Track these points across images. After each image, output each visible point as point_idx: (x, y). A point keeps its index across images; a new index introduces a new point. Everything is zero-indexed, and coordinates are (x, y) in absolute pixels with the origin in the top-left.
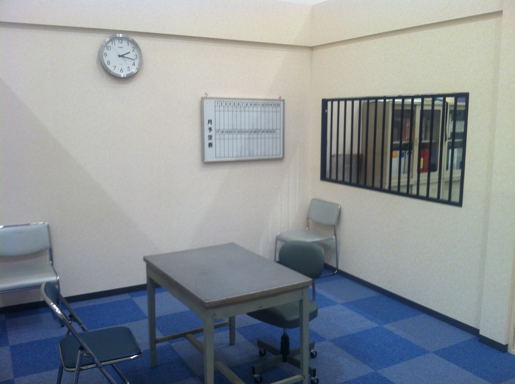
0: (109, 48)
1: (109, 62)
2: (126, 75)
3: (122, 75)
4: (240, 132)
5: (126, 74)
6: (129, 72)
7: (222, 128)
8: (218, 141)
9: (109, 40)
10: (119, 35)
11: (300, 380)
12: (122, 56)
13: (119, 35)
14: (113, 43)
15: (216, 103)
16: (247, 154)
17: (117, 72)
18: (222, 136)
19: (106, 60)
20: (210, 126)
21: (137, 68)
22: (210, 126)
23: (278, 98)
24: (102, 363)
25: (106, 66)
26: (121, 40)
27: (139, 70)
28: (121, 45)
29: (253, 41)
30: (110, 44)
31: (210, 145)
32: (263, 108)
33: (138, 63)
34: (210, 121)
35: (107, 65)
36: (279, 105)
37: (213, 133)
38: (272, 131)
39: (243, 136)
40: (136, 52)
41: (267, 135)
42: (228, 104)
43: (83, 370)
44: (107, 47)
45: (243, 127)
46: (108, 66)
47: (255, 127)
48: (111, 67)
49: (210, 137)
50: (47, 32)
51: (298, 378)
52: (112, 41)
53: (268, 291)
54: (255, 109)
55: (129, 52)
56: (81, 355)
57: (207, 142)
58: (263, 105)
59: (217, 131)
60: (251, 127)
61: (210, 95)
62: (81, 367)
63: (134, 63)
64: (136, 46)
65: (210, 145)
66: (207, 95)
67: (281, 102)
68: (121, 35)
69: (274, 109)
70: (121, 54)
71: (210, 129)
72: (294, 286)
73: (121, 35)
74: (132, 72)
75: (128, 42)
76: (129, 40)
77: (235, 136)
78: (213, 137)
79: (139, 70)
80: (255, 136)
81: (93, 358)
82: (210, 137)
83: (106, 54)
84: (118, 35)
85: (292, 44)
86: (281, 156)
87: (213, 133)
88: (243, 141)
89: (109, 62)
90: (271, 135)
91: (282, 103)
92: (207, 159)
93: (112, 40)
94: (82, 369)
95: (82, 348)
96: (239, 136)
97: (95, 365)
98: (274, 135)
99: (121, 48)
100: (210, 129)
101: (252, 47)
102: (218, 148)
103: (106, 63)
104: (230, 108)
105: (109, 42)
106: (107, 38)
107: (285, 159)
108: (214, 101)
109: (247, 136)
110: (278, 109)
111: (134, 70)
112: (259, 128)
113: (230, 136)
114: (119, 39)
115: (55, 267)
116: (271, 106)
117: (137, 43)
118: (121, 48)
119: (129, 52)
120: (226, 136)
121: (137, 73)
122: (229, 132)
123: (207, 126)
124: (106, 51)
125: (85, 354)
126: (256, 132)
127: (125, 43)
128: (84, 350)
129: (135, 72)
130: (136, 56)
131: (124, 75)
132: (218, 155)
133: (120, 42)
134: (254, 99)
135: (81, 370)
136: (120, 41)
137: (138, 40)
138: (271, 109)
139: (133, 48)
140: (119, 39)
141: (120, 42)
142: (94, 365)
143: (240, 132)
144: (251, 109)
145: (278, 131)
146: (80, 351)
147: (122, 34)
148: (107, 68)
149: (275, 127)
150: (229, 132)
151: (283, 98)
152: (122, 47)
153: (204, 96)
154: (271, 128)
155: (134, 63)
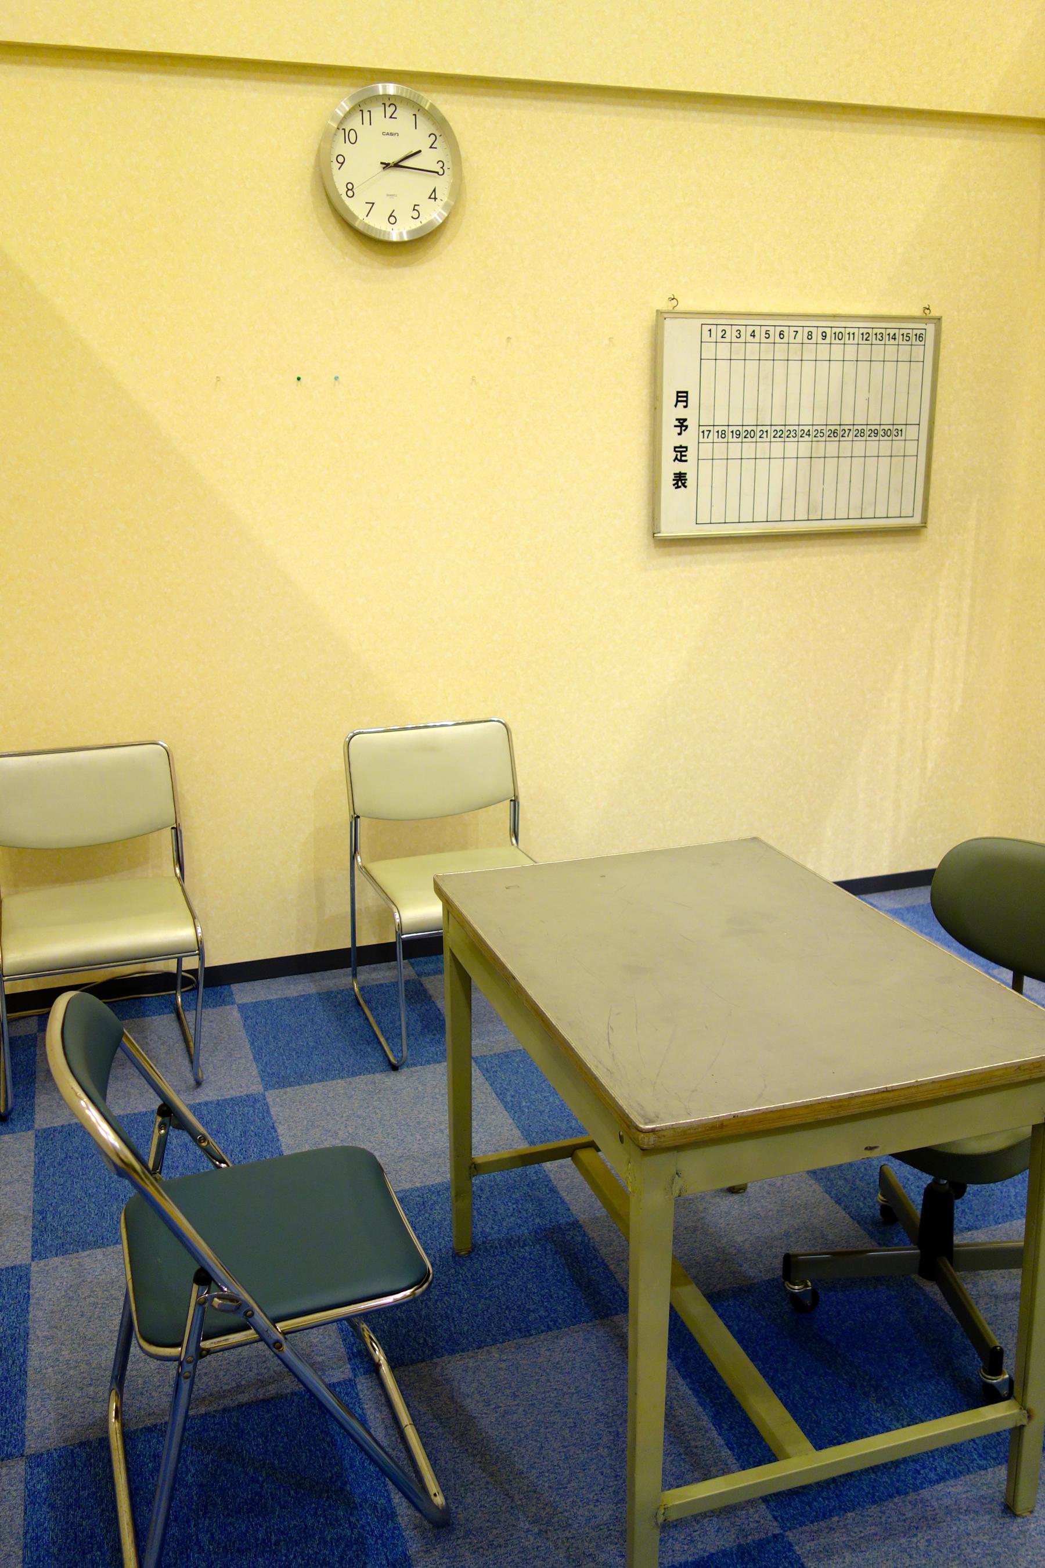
0: (352, 134)
1: (350, 189)
2: (409, 233)
3: (396, 233)
4: (783, 433)
5: (408, 229)
6: (416, 225)
7: (721, 420)
8: (705, 466)
9: (348, 109)
10: (384, 88)
11: (1010, 1425)
12: (397, 165)
13: (384, 88)
14: (366, 115)
15: (706, 328)
16: (802, 514)
17: (377, 223)
18: (720, 449)
19: (340, 179)
20: (681, 412)
21: (446, 206)
22: (681, 412)
23: (917, 312)
24: (279, 1326)
25: (342, 201)
26: (393, 108)
27: (453, 211)
28: (390, 125)
29: (842, 101)
30: (355, 123)
31: (680, 479)
32: (864, 349)
33: (446, 192)
34: (682, 397)
35: (344, 197)
36: (920, 337)
37: (688, 439)
38: (892, 432)
39: (791, 448)
40: (440, 153)
41: (873, 446)
42: (746, 333)
43: (209, 1352)
44: (344, 130)
45: (792, 419)
46: (348, 202)
47: (834, 419)
48: (356, 207)
49: (681, 452)
50: (145, 77)
51: (1005, 1417)
52: (362, 111)
53: (909, 1087)
54: (837, 351)
55: (420, 151)
56: (200, 1304)
57: (670, 468)
58: (866, 337)
59: (704, 432)
60: (820, 419)
61: (686, 304)
62: (205, 1339)
63: (434, 190)
64: (441, 129)
65: (680, 479)
66: (674, 302)
67: (929, 325)
68: (391, 89)
69: (905, 350)
70: (391, 160)
71: (682, 424)
72: (1019, 1068)
73: (391, 89)
74: (430, 223)
75: (415, 115)
76: (420, 108)
77: (763, 448)
78: (690, 455)
79: (453, 211)
80: (832, 447)
81: (249, 1314)
82: (681, 452)
83: (341, 159)
84: (380, 86)
85: (981, 109)
86: (916, 520)
87: (688, 439)
88: (790, 464)
89: (350, 186)
90: (885, 446)
91: (931, 328)
92: (667, 530)
93: (360, 107)
94: (204, 1352)
95: (204, 1278)
96: (777, 448)
97: (252, 1331)
98: (898, 445)
99: (392, 134)
100: (682, 424)
101: (837, 124)
102: (704, 491)
103: (342, 190)
104: (752, 350)
105: (348, 115)
106: (342, 103)
107: (930, 531)
108: (698, 322)
109: (804, 448)
110: (918, 351)
111: (433, 214)
112: (847, 419)
113: (749, 449)
114: (390, 102)
115: (186, 885)
116: (892, 341)
117: (447, 118)
118: (392, 134)
119: (420, 151)
120: (735, 449)
121: (445, 221)
122: (745, 434)
123: (671, 413)
124: (342, 147)
125: (216, 1299)
126: (835, 433)
127: (404, 116)
128: (213, 1284)
129: (441, 221)
130: (441, 164)
131: (401, 234)
132: (703, 517)
133: (388, 115)
134: (835, 317)
135: (202, 1353)
136: (390, 110)
137: (449, 105)
138: (891, 350)
139: (433, 138)
140: (390, 102)
141: (388, 115)
142: (249, 1334)
143: (783, 433)
144: (823, 351)
145: (911, 432)
146: (195, 1287)
147: (921, 1252)
148: (347, 208)
149: (900, 419)
150: (745, 434)
151: (935, 313)
152: (394, 132)
153: (664, 305)
154: (887, 419)
155: (434, 190)
